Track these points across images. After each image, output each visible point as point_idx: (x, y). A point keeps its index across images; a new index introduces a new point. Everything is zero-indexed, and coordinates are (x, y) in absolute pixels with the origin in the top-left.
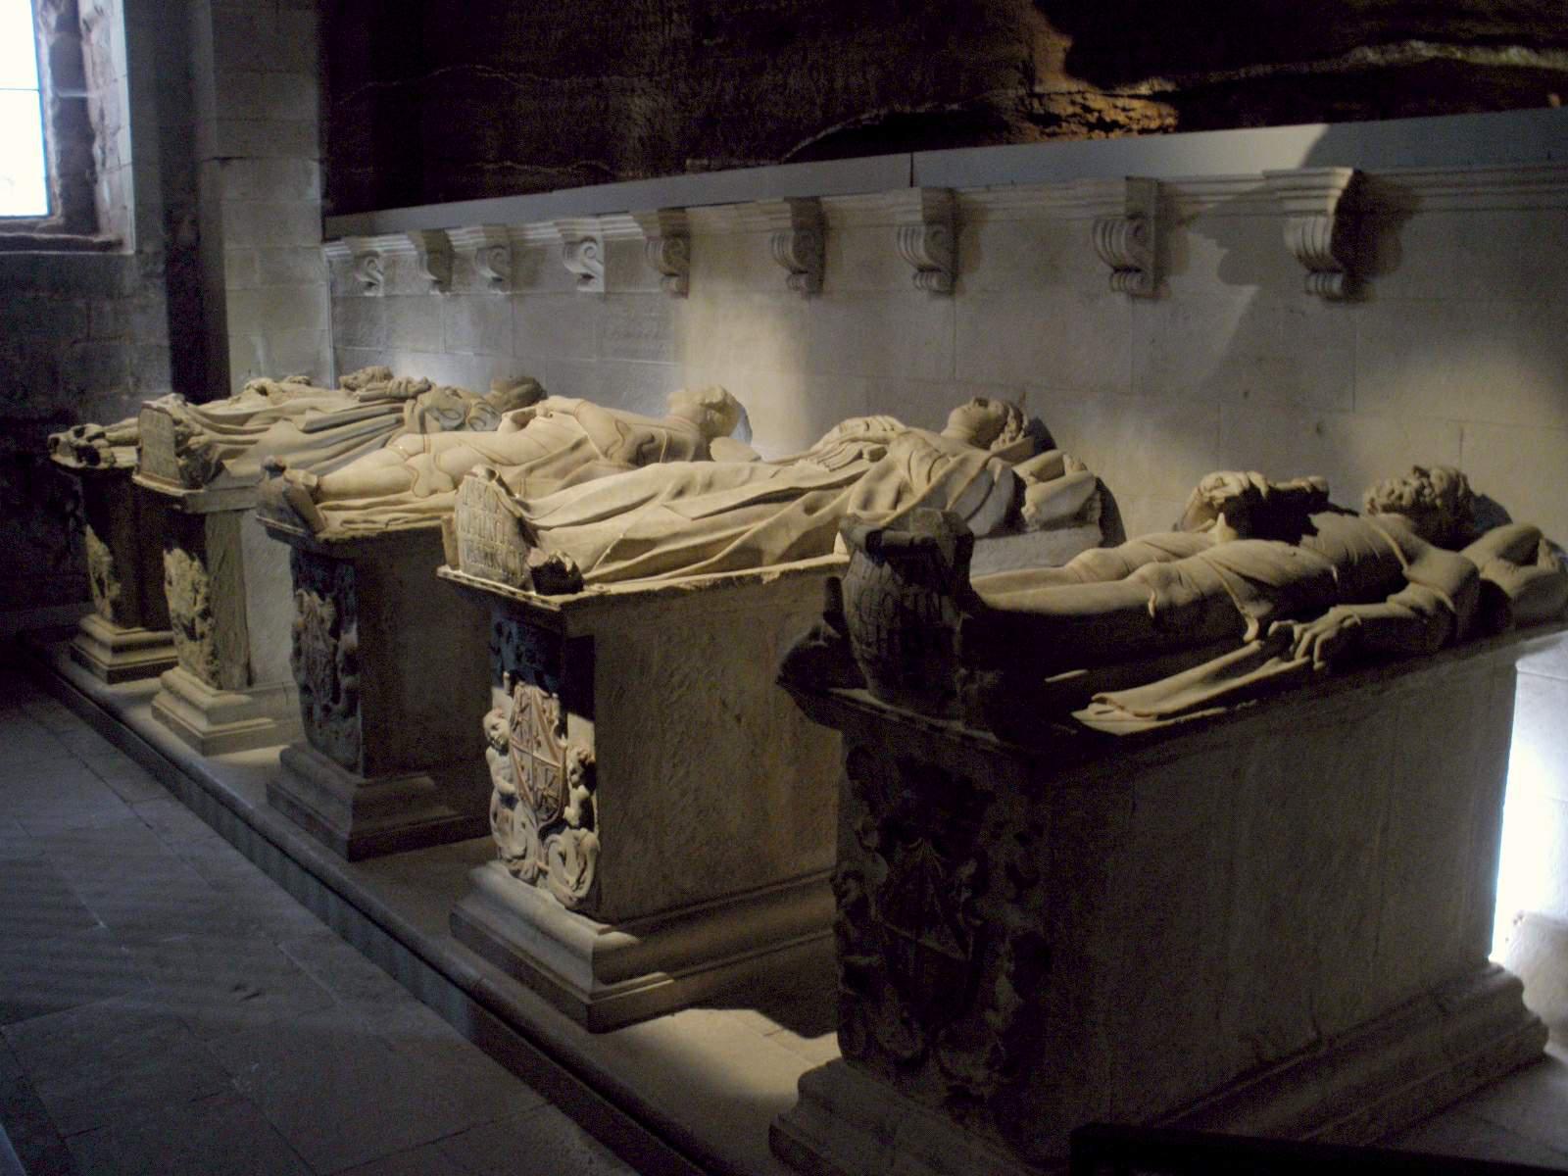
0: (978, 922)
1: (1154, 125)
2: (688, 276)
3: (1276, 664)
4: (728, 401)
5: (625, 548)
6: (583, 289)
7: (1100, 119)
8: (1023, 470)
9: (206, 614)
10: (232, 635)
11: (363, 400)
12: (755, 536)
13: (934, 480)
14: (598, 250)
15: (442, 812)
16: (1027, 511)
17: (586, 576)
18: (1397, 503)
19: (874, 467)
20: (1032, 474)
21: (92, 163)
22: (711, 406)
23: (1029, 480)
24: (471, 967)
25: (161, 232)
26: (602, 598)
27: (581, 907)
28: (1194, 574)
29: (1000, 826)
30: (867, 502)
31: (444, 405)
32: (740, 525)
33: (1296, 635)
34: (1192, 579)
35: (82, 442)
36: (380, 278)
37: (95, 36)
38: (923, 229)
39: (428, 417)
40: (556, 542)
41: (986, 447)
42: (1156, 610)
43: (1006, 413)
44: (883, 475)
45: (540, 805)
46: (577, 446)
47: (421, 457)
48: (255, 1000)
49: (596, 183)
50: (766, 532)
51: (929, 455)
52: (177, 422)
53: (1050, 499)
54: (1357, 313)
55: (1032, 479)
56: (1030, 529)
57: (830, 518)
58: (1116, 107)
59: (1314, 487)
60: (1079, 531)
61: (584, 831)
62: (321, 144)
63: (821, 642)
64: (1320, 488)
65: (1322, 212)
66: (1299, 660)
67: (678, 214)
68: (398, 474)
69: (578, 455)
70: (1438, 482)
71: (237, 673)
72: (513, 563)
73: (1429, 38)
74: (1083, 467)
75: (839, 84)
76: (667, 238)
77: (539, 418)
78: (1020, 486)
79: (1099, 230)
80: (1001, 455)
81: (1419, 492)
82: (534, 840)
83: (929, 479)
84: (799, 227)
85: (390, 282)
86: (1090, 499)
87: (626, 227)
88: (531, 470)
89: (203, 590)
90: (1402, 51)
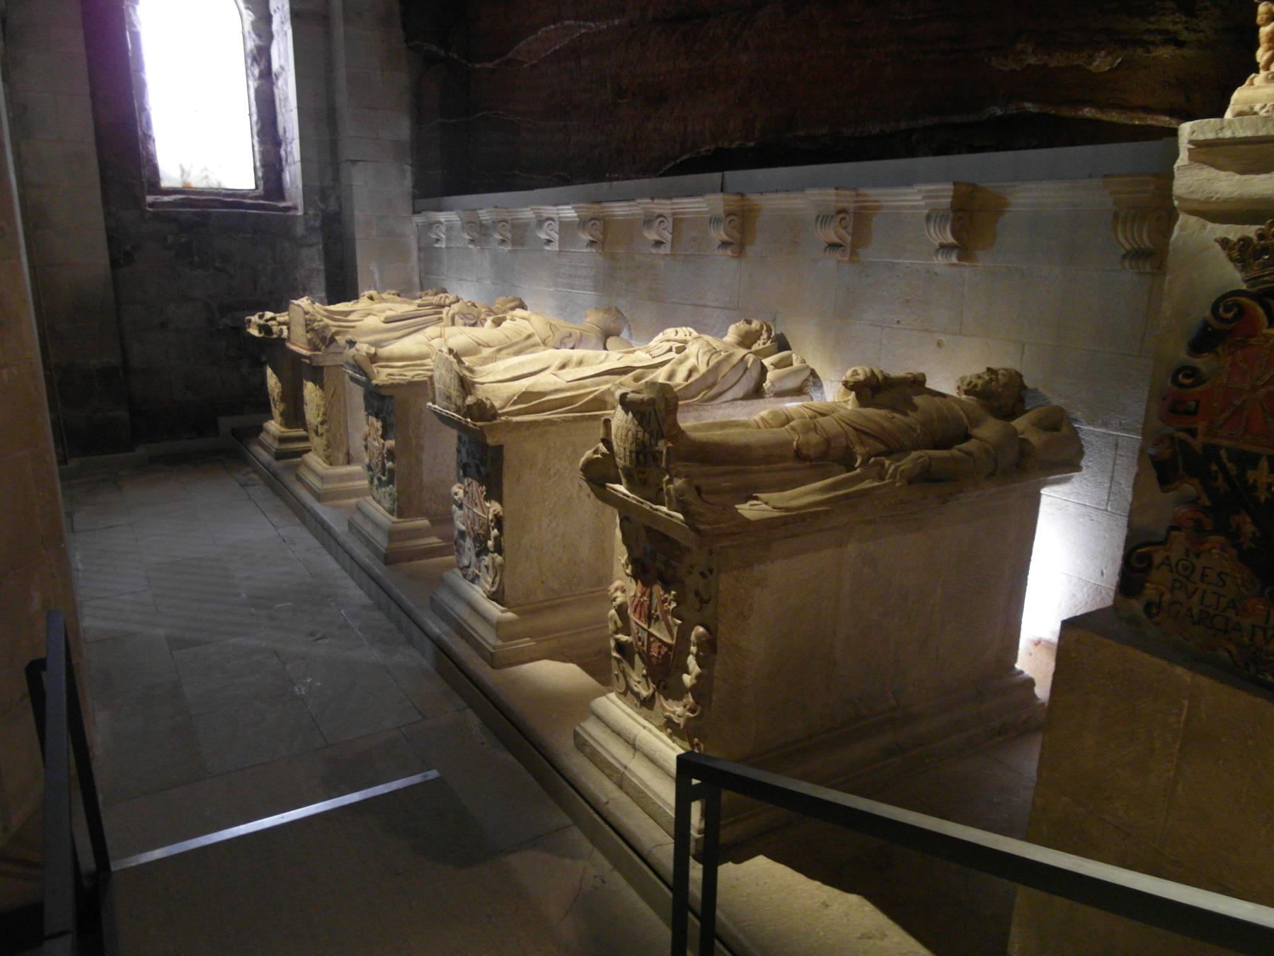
5: (526, 396)
6: (547, 248)
8: (767, 362)
9: (322, 423)
11: (419, 306)
14: (556, 226)
15: (434, 541)
16: (767, 385)
19: (677, 356)
21: (281, 160)
23: (770, 368)
24: (437, 627)
26: (507, 423)
29: (692, 566)
30: (671, 376)
31: (466, 311)
35: (262, 322)
37: (280, 82)
39: (456, 317)
40: (485, 391)
41: (749, 347)
43: (762, 327)
44: (681, 362)
46: (529, 337)
47: (437, 340)
52: (306, 313)
53: (780, 379)
68: (425, 349)
71: (341, 456)
72: (459, 402)
74: (803, 361)
75: (690, 128)
78: (764, 370)
80: (756, 353)
82: (474, 558)
85: (448, 239)
86: (806, 380)
88: (500, 350)
89: (322, 410)
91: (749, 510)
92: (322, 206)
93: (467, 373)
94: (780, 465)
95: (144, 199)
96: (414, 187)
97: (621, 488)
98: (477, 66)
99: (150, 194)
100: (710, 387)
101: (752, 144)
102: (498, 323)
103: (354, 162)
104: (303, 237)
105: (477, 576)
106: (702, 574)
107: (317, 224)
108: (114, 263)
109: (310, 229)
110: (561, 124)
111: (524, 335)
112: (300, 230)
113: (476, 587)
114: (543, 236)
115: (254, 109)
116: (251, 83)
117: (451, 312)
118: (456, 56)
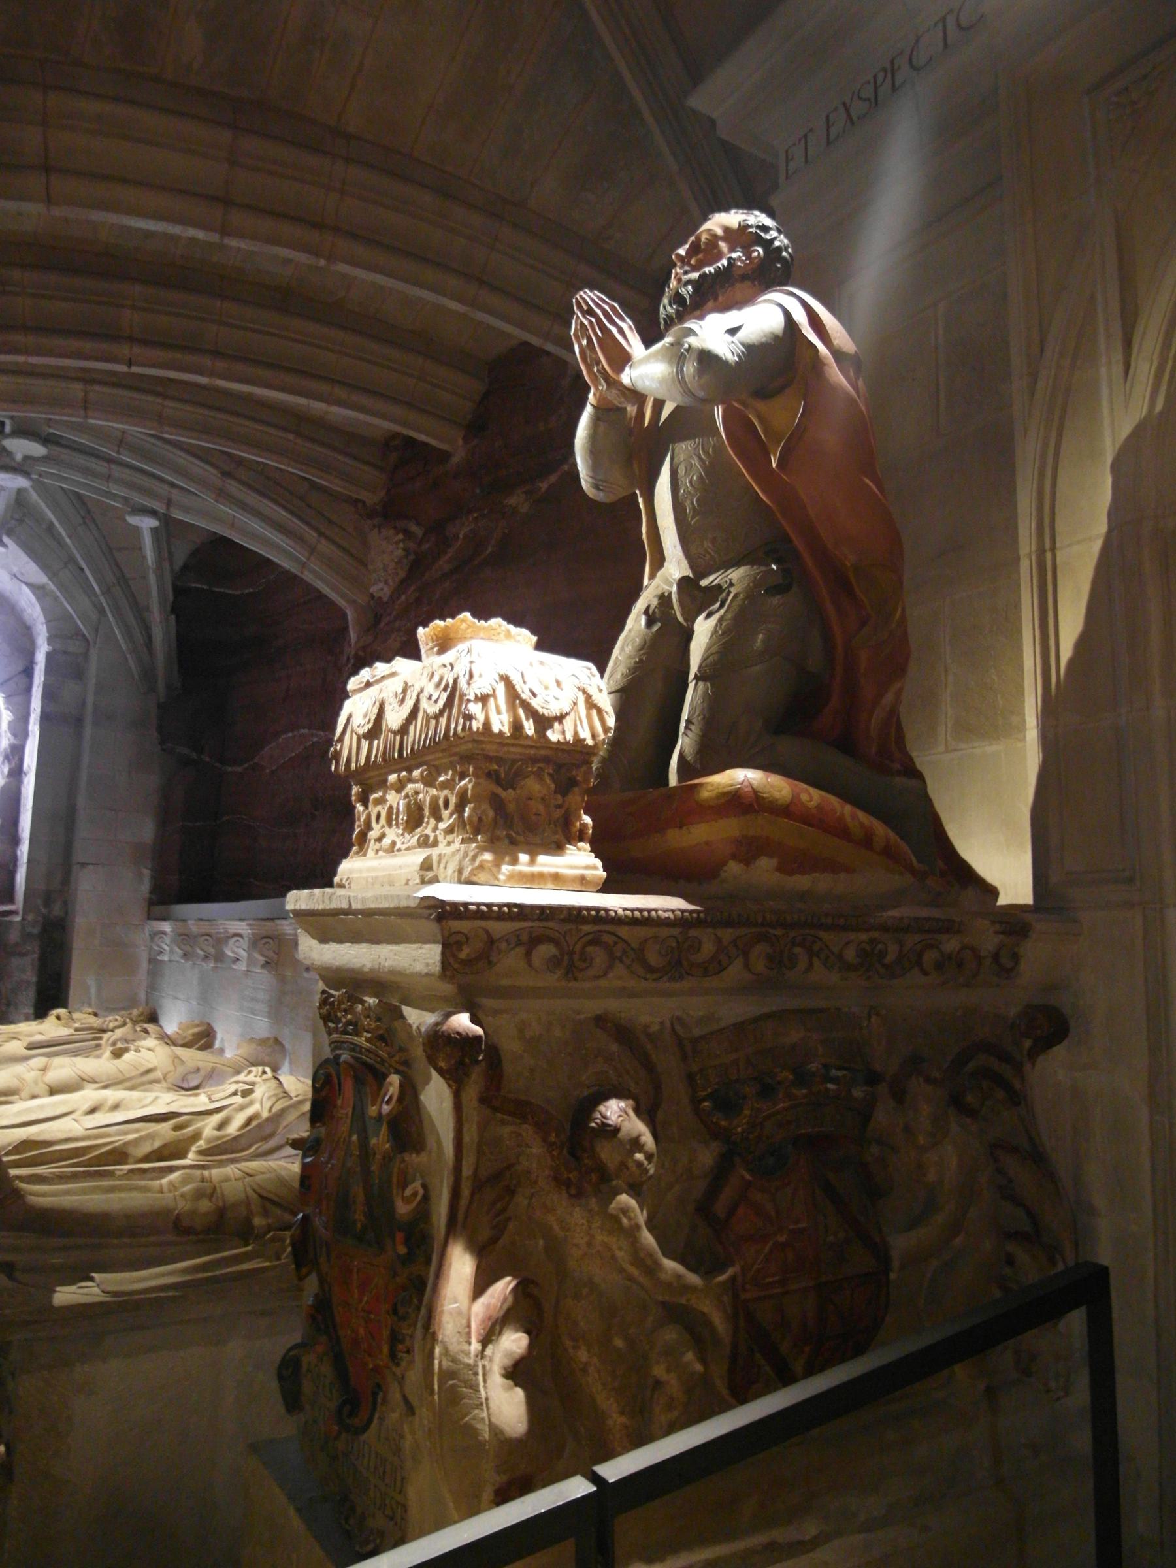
11: (76, 1030)
12: (126, 1144)
13: (274, 1110)
28: (226, 1193)
30: (221, 1126)
36: (166, 948)
44: (242, 1108)
46: (149, 1071)
50: (136, 1142)
91: (66, 1295)
92: (44, 911)
94: (151, 1239)
96: (151, 893)
98: (229, 769)
100: (265, 1139)
102: (118, 1054)
103: (84, 865)
104: (17, 944)
107: (36, 931)
109: (26, 937)
111: (142, 1070)
112: (14, 936)
118: (207, 759)
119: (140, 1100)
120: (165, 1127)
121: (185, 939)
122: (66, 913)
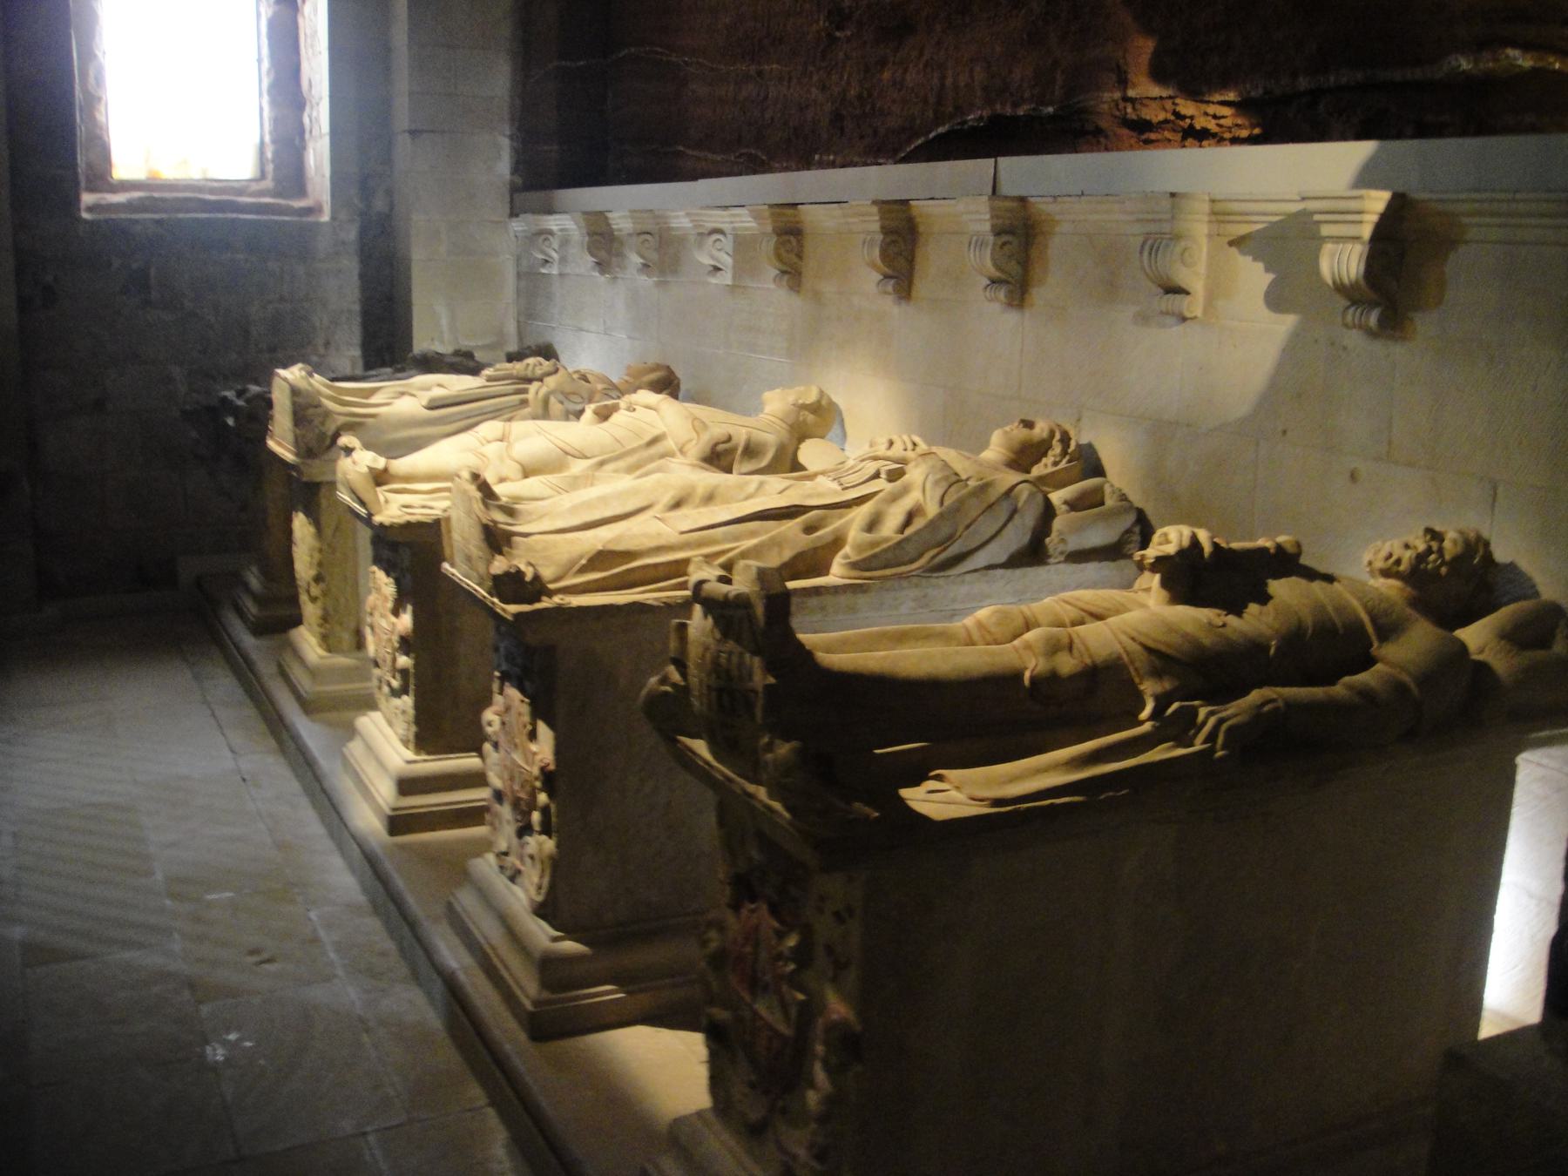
0: (801, 997)
1: (1244, 133)
2: (800, 274)
3: (1170, 749)
4: (824, 402)
5: (601, 558)
6: (713, 281)
7: (1191, 126)
10: (342, 600)
11: (490, 379)
13: (947, 502)
14: (727, 243)
16: (1051, 542)
17: (551, 586)
18: (1395, 568)
19: (889, 487)
20: (1066, 502)
22: (804, 407)
25: (356, 201)
26: (560, 610)
27: (543, 911)
29: (822, 899)
30: (872, 525)
31: (568, 389)
32: (730, 541)
33: (1201, 717)
34: (1087, 649)
36: (555, 255)
38: (991, 238)
39: (552, 400)
40: (530, 549)
42: (1033, 679)
45: (516, 804)
46: (654, 441)
48: (266, 966)
49: (755, 172)
51: (946, 478)
54: (1398, 350)
55: (1064, 507)
56: (1052, 560)
57: (830, 538)
58: (1206, 114)
59: (1279, 547)
60: (1112, 565)
61: (544, 837)
62: (512, 120)
63: (668, 689)
64: (1290, 549)
65: (1356, 239)
66: (1198, 746)
67: (790, 212)
69: (653, 450)
70: (1450, 547)
73: (1526, 47)
75: (949, 81)
76: (779, 235)
77: (622, 412)
78: (1049, 511)
79: (1147, 248)
80: (1041, 480)
81: (1421, 558)
82: (515, 841)
83: (942, 503)
84: (886, 231)
85: (563, 260)
86: (1128, 531)
87: (745, 221)
88: (602, 464)
90: (1496, 60)
93: (499, 517)
95: (78, 199)
97: (700, 747)
99: (92, 190)
101: (1051, 109)
102: (604, 415)
105: (519, 872)
106: (837, 915)
108: (24, 304)
110: (753, 68)
111: (647, 438)
113: (516, 888)
114: (707, 261)
115: (265, 51)
116: (263, 10)
117: (544, 390)
119: (741, 487)
120: (792, 527)
121: (604, 244)
122: (392, 207)
